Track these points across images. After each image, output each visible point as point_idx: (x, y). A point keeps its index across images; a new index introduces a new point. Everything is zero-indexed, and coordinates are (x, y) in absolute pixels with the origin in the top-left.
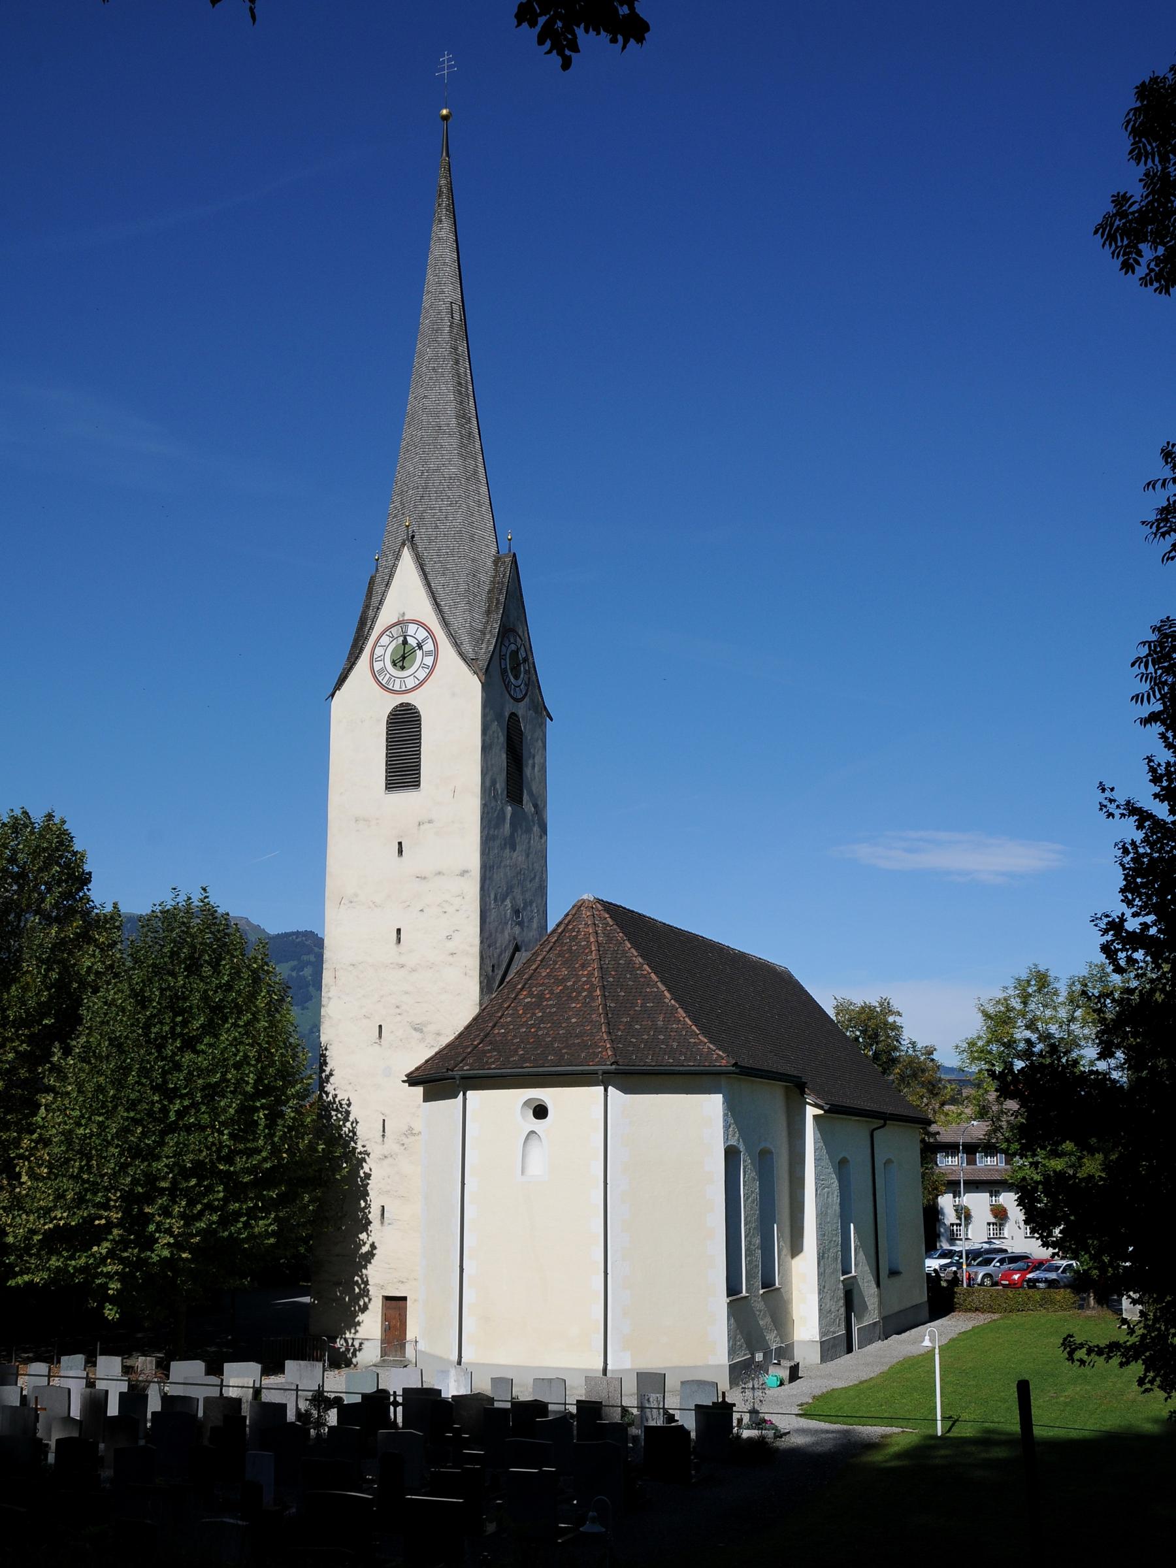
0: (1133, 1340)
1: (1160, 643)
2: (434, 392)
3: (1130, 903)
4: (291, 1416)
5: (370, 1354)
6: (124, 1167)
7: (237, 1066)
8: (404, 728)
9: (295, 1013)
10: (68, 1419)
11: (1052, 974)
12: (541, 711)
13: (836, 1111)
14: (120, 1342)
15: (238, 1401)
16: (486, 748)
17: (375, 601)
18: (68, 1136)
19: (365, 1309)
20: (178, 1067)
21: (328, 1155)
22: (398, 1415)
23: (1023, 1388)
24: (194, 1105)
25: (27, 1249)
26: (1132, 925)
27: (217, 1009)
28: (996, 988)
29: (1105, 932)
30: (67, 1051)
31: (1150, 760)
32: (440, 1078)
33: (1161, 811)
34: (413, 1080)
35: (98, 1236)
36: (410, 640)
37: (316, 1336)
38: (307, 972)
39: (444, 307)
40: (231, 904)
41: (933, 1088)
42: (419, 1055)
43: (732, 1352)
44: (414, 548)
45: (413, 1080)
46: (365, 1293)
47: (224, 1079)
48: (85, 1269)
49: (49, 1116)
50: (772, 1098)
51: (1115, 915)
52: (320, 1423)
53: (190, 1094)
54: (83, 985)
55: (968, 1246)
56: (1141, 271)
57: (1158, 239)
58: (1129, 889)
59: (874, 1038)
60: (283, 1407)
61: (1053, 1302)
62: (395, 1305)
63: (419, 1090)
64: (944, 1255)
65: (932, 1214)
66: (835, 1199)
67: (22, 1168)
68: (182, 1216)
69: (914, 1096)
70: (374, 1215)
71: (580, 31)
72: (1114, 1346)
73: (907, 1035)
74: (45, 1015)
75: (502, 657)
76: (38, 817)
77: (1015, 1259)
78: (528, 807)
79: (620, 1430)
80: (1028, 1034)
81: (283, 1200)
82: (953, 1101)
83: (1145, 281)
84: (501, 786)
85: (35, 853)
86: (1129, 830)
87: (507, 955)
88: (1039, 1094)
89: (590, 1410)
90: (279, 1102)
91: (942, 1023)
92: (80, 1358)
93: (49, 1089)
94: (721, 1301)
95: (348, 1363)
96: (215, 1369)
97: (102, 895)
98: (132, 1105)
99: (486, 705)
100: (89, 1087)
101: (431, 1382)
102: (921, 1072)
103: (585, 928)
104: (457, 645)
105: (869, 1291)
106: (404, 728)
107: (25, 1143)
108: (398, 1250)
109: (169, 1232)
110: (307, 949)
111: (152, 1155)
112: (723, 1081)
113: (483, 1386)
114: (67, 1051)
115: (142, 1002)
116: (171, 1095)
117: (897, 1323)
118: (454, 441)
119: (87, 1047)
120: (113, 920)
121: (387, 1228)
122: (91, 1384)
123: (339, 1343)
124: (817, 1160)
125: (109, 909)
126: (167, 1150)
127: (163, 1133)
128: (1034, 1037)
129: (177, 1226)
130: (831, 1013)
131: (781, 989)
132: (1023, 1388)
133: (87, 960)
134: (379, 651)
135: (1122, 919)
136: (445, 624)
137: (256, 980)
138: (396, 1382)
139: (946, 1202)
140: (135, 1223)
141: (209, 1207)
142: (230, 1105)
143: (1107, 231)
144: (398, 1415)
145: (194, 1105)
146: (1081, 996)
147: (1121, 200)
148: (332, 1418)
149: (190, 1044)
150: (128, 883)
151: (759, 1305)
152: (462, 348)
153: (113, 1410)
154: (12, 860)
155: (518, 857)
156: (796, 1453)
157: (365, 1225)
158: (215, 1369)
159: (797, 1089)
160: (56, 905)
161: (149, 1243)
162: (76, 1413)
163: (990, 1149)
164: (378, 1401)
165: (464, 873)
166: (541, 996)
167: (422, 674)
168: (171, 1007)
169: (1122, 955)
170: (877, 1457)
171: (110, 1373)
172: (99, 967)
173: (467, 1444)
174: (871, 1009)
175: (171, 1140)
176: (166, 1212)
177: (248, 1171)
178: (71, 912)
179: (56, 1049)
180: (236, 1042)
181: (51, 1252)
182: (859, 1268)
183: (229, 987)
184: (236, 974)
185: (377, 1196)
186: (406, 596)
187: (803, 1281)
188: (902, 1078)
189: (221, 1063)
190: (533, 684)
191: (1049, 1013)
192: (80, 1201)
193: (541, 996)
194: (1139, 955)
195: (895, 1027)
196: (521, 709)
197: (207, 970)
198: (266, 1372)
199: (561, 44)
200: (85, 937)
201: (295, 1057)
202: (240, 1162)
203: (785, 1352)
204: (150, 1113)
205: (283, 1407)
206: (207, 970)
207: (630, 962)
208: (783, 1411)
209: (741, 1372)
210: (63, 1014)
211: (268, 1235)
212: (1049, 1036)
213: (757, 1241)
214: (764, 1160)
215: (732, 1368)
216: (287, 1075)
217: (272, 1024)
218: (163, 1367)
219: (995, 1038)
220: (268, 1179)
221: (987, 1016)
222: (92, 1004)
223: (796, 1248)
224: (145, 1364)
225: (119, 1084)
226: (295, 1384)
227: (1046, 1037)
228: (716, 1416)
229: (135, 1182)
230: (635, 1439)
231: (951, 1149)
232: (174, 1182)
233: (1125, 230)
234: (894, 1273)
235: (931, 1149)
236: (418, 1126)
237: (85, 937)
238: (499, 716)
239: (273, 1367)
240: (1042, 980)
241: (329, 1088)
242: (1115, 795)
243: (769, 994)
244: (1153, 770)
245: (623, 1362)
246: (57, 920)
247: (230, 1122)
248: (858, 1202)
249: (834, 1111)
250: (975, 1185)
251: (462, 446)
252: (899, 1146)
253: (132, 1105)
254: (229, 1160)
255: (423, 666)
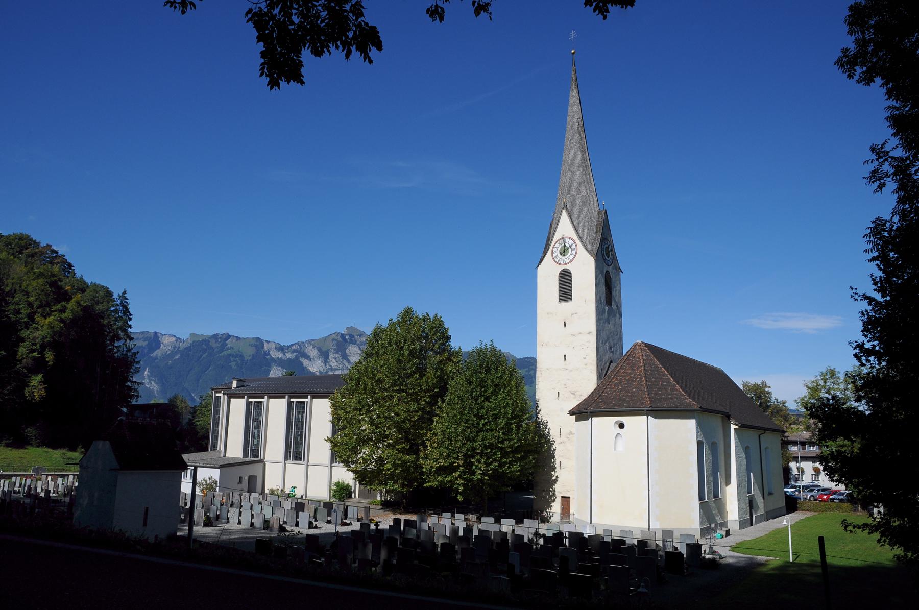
0: (874, 523)
1: (876, 227)
2: (573, 151)
3: (866, 336)
4: (526, 540)
5: (556, 518)
6: (464, 444)
7: (505, 407)
8: (565, 278)
9: (527, 388)
10: (445, 536)
11: (837, 370)
12: (618, 269)
13: (743, 427)
14: (464, 509)
15: (506, 533)
16: (597, 285)
17: (553, 230)
18: (444, 432)
19: (554, 501)
20: (483, 407)
21: (539, 442)
22: (567, 542)
23: (821, 540)
24: (489, 422)
25: (430, 473)
26: (868, 345)
27: (497, 386)
28: (812, 375)
29: (855, 348)
30: (443, 401)
31: (872, 275)
32: (582, 412)
33: (878, 297)
34: (571, 413)
35: (455, 469)
36: (567, 245)
37: (534, 510)
38: (532, 372)
39: (575, 120)
40: (503, 347)
41: (786, 418)
42: (574, 403)
43: (701, 523)
44: (567, 210)
45: (571, 413)
46: (554, 495)
47: (500, 412)
48: (450, 482)
49: (438, 425)
50: (717, 421)
51: (859, 342)
52: (537, 544)
53: (488, 418)
54: (448, 377)
55: (803, 484)
56: (856, 77)
57: (863, 64)
58: (865, 330)
59: (760, 397)
60: (523, 536)
61: (842, 508)
62: (566, 500)
63: (574, 417)
64: (792, 487)
65: (787, 471)
66: (744, 462)
67: (428, 443)
68: (485, 463)
69: (778, 422)
70: (557, 465)
71: (609, 6)
72: (865, 526)
73: (774, 396)
74: (434, 388)
75: (602, 249)
76: (432, 316)
77: (824, 490)
78: (614, 307)
79: (655, 552)
80: (827, 395)
81: (522, 458)
82: (795, 423)
83: (858, 81)
84: (603, 299)
85: (431, 329)
86: (865, 306)
87: (607, 365)
88: (828, 416)
89: (643, 543)
90: (520, 421)
91: (789, 390)
92: (449, 514)
93: (437, 415)
94: (697, 502)
95: (548, 521)
96: (498, 521)
97: (455, 343)
98: (466, 422)
99: (596, 268)
100: (451, 414)
101: (580, 530)
102: (780, 411)
103: (638, 353)
104: (584, 246)
105: (760, 501)
106: (565, 278)
107: (429, 435)
108: (567, 478)
109: (480, 469)
110: (530, 364)
111: (473, 440)
112: (696, 414)
113: (600, 532)
114: (443, 401)
115: (470, 383)
116: (481, 418)
117: (772, 515)
118: (581, 169)
119: (450, 400)
120: (458, 353)
121: (562, 470)
122: (453, 524)
123: (545, 513)
124: (736, 446)
125: (457, 349)
126: (480, 439)
127: (478, 432)
128: (830, 397)
129: (483, 467)
130: (741, 387)
131: (718, 378)
132: (821, 540)
133: (450, 368)
134: (555, 249)
135: (863, 343)
136: (580, 238)
137: (511, 375)
138: (566, 529)
139: (793, 465)
140: (468, 465)
141: (495, 460)
142: (502, 422)
143: (840, 63)
144: (567, 542)
145: (489, 422)
146: (851, 378)
147: (845, 51)
148: (541, 541)
149: (487, 399)
150: (464, 340)
151: (713, 505)
152: (583, 134)
153: (461, 534)
154: (423, 331)
155: (611, 326)
156: (728, 565)
157: (554, 469)
158: (498, 521)
159: (727, 417)
160: (439, 348)
161: (473, 473)
162: (448, 534)
163: (812, 444)
164: (559, 536)
165: (590, 333)
166: (621, 380)
167: (571, 257)
168: (480, 385)
169: (864, 358)
170: (764, 569)
171: (460, 522)
172: (454, 370)
173: (593, 554)
174: (758, 385)
175: (481, 435)
176: (479, 462)
177: (509, 447)
178: (444, 350)
179: (439, 400)
180: (504, 398)
181: (439, 475)
182: (755, 491)
183: (501, 377)
184: (504, 372)
185: (558, 458)
186: (565, 228)
187: (731, 495)
188: (772, 413)
189: (498, 406)
190: (615, 259)
191: (836, 386)
192: (449, 456)
193: (621, 380)
194: (871, 358)
195: (768, 393)
196: (610, 269)
197: (493, 371)
198: (516, 523)
199: (603, 11)
200: (449, 359)
201: (526, 404)
202: (506, 444)
203: (724, 524)
204: (473, 425)
205: (523, 536)
206: (493, 371)
207: (656, 367)
208: (723, 549)
209: (705, 532)
210: (441, 389)
211: (517, 471)
212: (837, 396)
213: (711, 479)
214: (713, 447)
215: (701, 530)
216: (523, 411)
217: (517, 392)
218: (479, 520)
219: (812, 397)
220: (516, 450)
221: (808, 388)
222: (452, 383)
223: (728, 482)
224: (472, 517)
225: (462, 414)
226: (527, 529)
227: (834, 397)
228: (695, 548)
229: (468, 450)
230: (661, 556)
231: (794, 443)
232: (482, 451)
233: (847, 62)
234: (770, 494)
235: (785, 443)
236: (574, 431)
237: (449, 359)
238: (602, 272)
239: (519, 521)
240: (833, 373)
241: (539, 416)
242: (857, 291)
243: (717, 379)
244: (873, 280)
245: (656, 525)
246: (439, 353)
247: (503, 428)
248: (754, 463)
249: (743, 427)
250: (805, 459)
251: (584, 171)
252: (771, 442)
253: (466, 422)
254: (502, 442)
255: (572, 254)
